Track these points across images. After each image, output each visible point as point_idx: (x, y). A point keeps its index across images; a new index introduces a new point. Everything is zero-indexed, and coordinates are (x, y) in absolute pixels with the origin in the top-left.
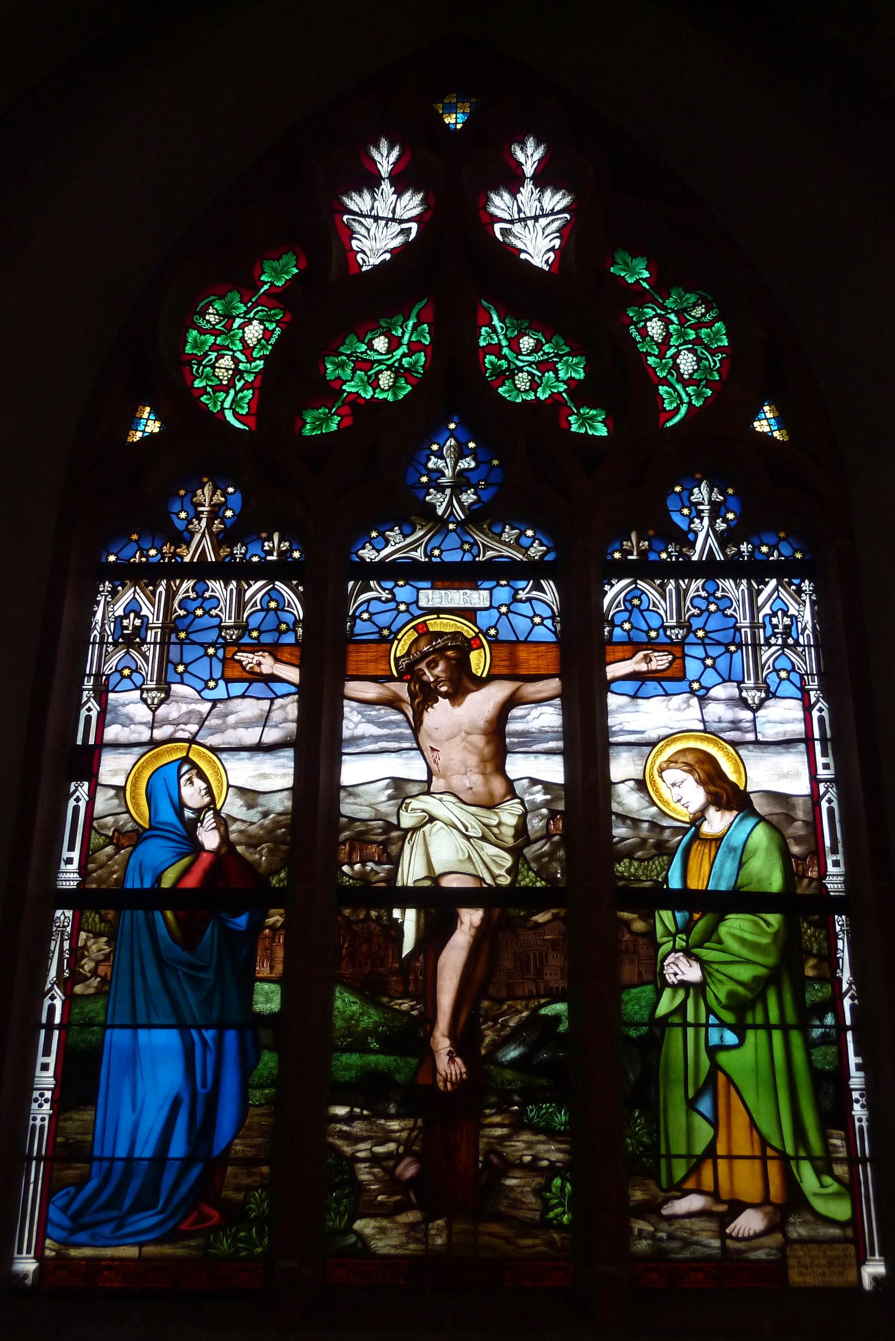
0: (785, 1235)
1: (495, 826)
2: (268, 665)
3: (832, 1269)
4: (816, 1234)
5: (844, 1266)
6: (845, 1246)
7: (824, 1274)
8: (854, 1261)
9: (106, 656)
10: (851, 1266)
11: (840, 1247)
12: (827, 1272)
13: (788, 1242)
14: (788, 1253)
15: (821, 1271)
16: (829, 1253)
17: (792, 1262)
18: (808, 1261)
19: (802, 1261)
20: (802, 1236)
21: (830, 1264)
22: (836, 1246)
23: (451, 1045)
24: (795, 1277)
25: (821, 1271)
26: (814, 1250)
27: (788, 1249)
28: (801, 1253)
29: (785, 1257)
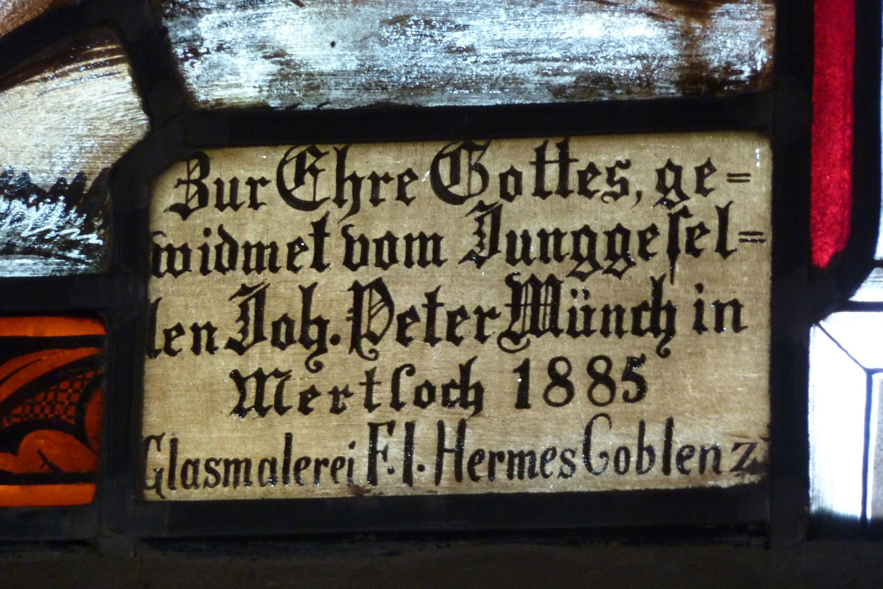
0: (158, 78)
1: (483, 216)
2: (406, 223)
3: (542, 350)
4: (431, 59)
5: (655, 315)
6: (687, 152)
7: (466, 391)
8: (748, 277)
9: (370, 309)
10: (728, 315)
11: (645, 158)
12: (493, 367)
13: (183, 128)
14: (169, 229)
15: (438, 363)
16: (527, 216)
17: (184, 299)
18: (334, 289)
19: (283, 295)
20: (314, 82)
21: (533, 307)
22: (602, 153)
23: (19, 199)
24: (199, 422)
25: (438, 363)
26: (399, 190)
27: (170, 195)
28: (275, 223)
29: (133, 253)
